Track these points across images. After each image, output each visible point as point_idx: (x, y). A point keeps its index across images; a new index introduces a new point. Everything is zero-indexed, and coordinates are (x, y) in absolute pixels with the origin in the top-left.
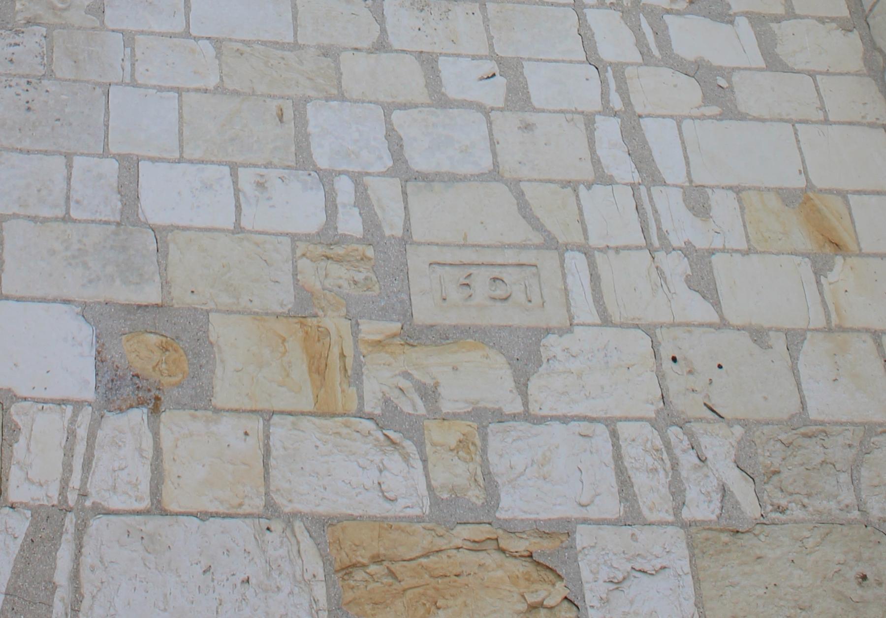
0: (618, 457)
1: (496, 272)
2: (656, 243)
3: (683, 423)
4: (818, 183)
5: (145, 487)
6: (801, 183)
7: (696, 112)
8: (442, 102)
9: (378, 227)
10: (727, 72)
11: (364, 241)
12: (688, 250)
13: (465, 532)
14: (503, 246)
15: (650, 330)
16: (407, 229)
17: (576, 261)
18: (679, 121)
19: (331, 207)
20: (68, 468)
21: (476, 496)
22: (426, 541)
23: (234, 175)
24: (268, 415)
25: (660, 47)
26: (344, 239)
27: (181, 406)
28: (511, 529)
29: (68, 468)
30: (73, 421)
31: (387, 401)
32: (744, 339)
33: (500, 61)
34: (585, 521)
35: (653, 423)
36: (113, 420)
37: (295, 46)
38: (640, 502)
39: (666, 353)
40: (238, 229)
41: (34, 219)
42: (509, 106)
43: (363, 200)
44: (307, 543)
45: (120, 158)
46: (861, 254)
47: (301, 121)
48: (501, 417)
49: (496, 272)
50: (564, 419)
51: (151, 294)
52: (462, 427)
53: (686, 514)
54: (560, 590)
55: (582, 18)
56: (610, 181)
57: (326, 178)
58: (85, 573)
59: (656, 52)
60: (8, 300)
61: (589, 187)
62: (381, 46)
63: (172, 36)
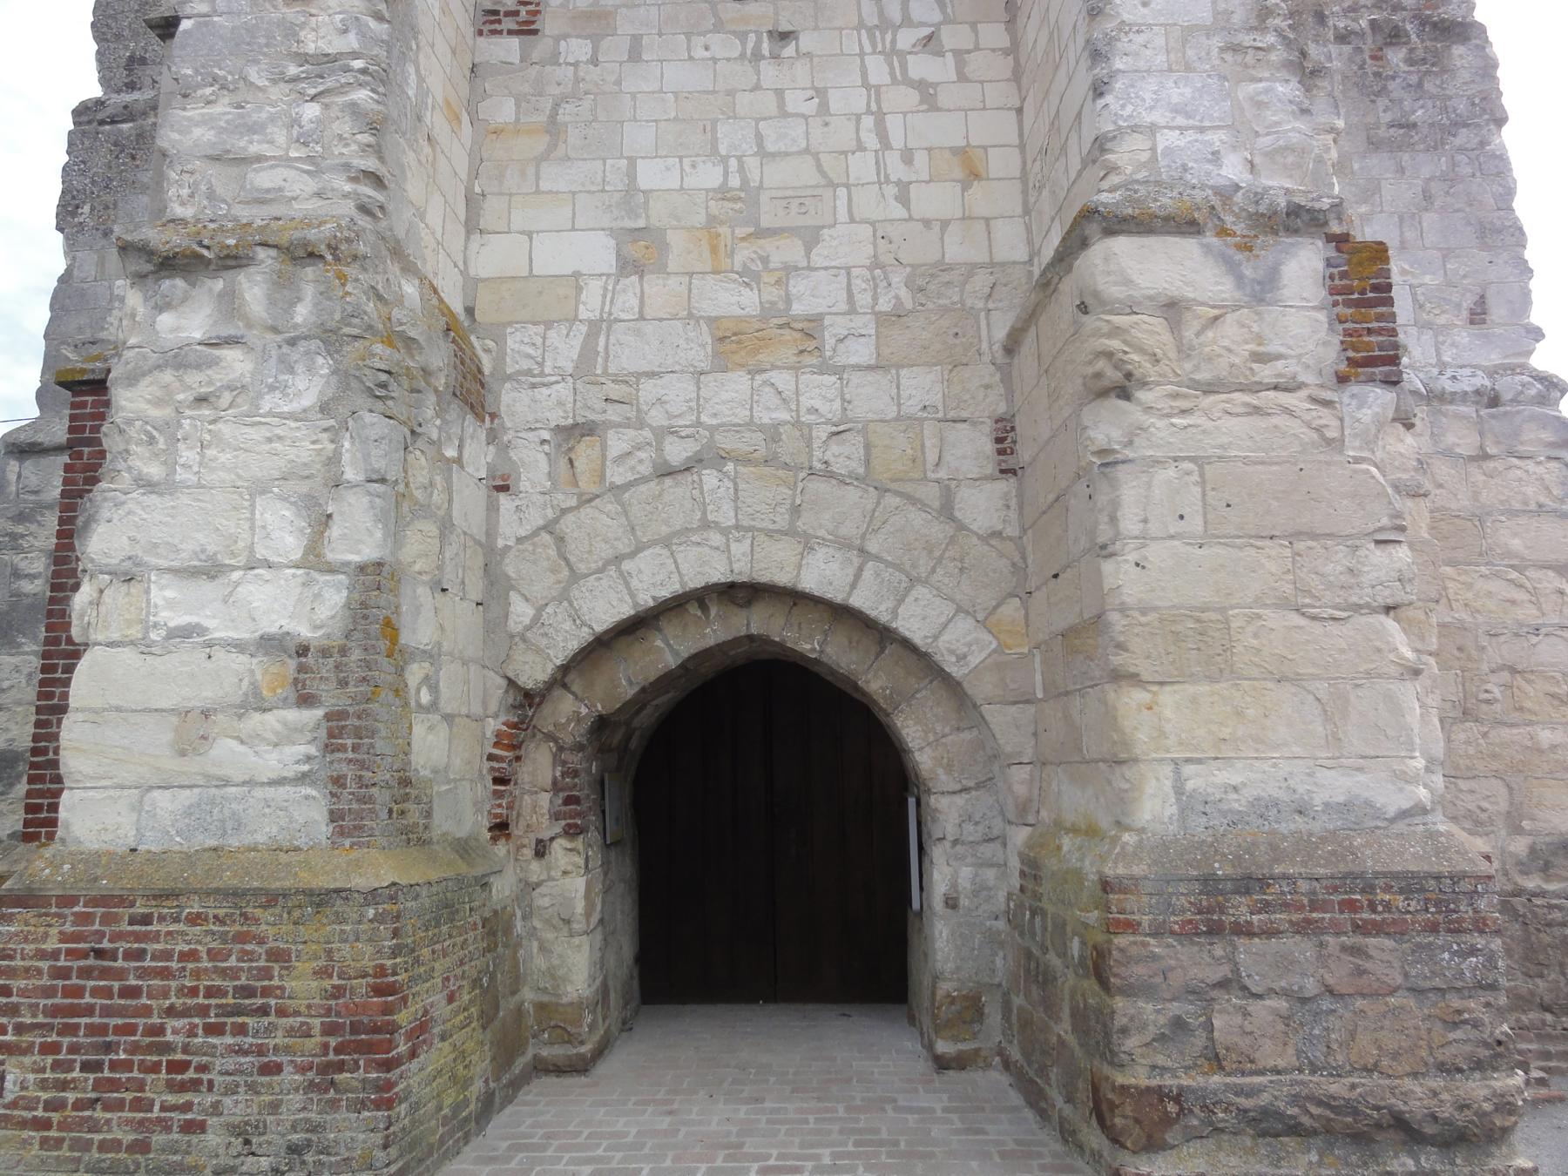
0: (849, 285)
1: (802, 200)
2: (882, 180)
3: (882, 267)
4: (973, 142)
5: (637, 310)
6: (964, 143)
7: (914, 109)
8: (784, 114)
9: (748, 182)
10: (935, 85)
11: (741, 189)
13: (775, 321)
14: (807, 187)
15: (873, 224)
16: (761, 182)
17: (842, 192)
18: (905, 114)
19: (726, 174)
20: (604, 303)
21: (781, 306)
22: (758, 326)
23: (681, 162)
24: (691, 274)
25: (902, 74)
26: (732, 189)
27: (652, 272)
28: (795, 318)
29: (604, 303)
30: (606, 283)
31: (745, 265)
32: (920, 226)
33: (817, 90)
34: (830, 314)
35: (868, 268)
36: (624, 282)
37: (714, 92)
39: (879, 234)
40: (682, 188)
41: (589, 192)
42: (819, 114)
43: (741, 169)
44: (705, 328)
45: (628, 158)
46: (988, 179)
47: (714, 130)
48: (796, 269)
49: (802, 200)
50: (826, 268)
51: (641, 223)
52: (778, 274)
53: (877, 308)
54: (814, 344)
55: (862, 61)
56: (865, 149)
58: (611, 347)
59: (899, 78)
61: (853, 153)
62: (757, 87)
63: (653, 92)
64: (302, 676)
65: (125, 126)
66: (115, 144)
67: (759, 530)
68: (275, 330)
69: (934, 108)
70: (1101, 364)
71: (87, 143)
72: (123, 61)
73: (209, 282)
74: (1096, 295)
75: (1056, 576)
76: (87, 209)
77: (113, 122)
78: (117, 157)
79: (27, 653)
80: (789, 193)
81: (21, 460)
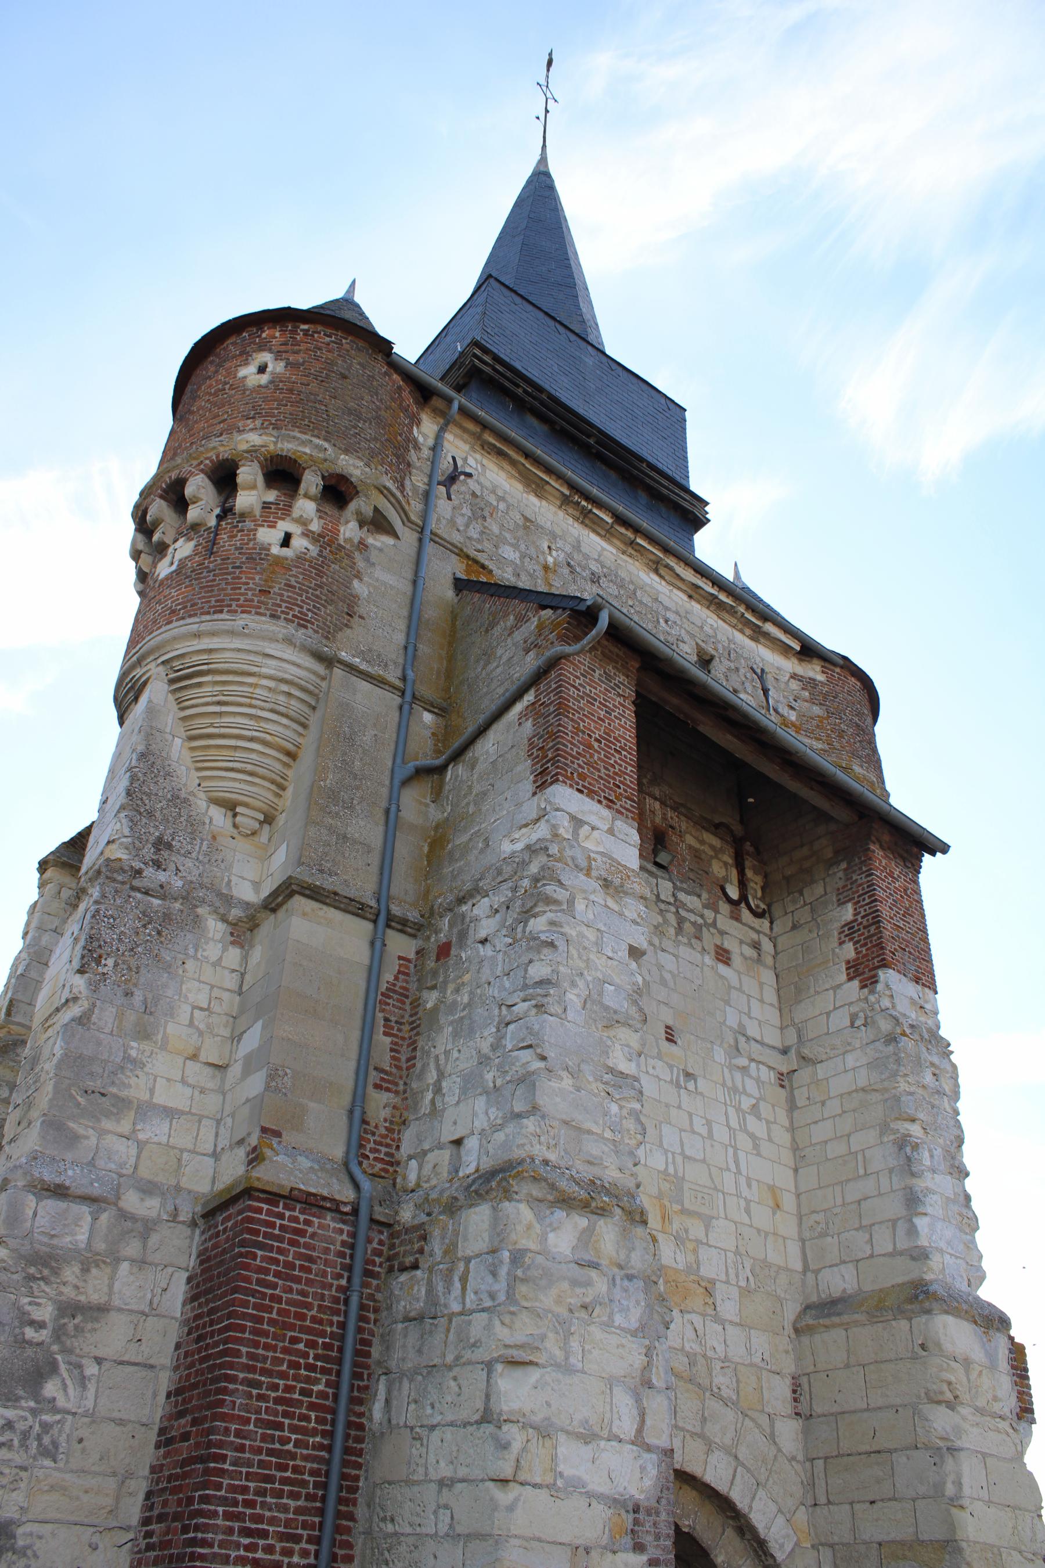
10: (759, 1139)
12: (745, 1199)
15: (735, 1223)
17: (721, 1195)
38: (399, 378)
48: (702, 1243)
50: (716, 1247)
57: (666, 1151)
60: (39, 888)
64: (636, 1528)
65: (156, 902)
66: (144, 913)
67: (688, 1431)
68: (620, 1267)
69: (759, 1154)
70: (945, 1387)
71: (118, 901)
72: (152, 839)
73: (577, 1218)
74: (938, 1345)
75: (872, 1502)
76: (110, 962)
77: (146, 893)
78: (144, 926)
79: (22, 1408)
80: (697, 1188)
81: (39, 1199)
